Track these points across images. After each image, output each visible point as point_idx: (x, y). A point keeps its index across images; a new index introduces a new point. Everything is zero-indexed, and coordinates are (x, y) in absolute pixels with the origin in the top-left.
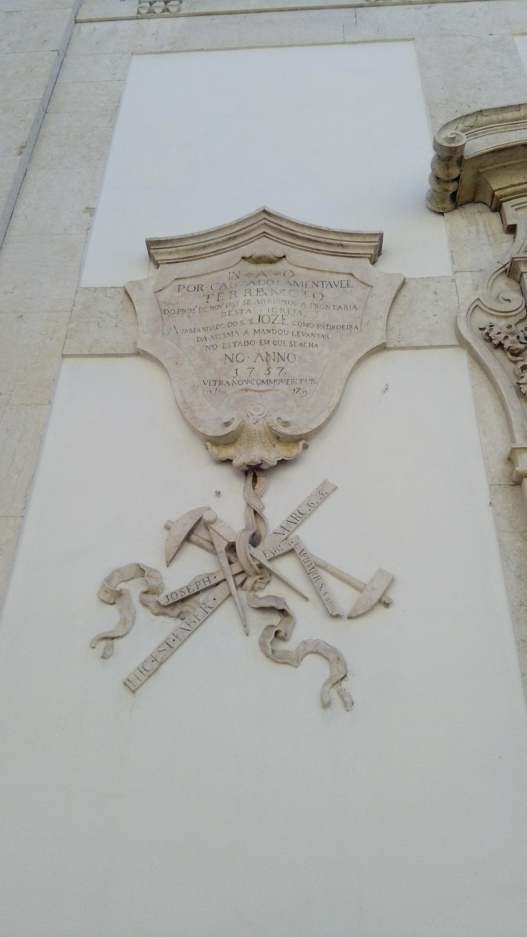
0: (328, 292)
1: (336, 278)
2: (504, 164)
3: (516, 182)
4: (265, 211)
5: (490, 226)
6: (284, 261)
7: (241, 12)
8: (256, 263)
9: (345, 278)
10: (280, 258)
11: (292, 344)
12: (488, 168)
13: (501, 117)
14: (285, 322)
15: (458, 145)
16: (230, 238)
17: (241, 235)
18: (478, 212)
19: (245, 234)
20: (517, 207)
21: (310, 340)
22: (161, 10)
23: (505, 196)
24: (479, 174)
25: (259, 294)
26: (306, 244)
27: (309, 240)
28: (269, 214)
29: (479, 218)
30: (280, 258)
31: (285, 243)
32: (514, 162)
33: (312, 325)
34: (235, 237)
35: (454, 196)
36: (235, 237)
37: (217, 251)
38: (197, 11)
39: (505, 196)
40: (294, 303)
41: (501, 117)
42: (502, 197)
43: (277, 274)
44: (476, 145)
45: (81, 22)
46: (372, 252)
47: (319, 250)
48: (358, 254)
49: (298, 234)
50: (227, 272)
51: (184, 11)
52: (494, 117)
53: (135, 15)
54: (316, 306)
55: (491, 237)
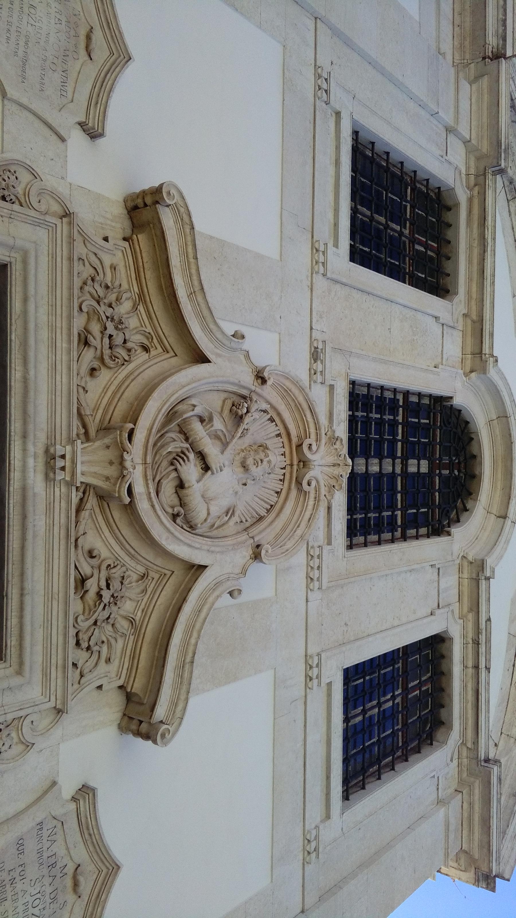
0: (57, 77)
1: (70, 89)
2: (156, 245)
3: (144, 255)
4: (130, 59)
5: (110, 230)
6: (87, 58)
7: (314, 145)
8: (87, 36)
9: (70, 95)
10: (90, 56)
11: (9, 23)
12: (153, 231)
13: (189, 243)
14: (29, 25)
15: (166, 199)
16: (108, 23)
17: (111, 33)
18: (124, 228)
19: (112, 36)
20: (124, 252)
21: (13, 39)
22: (320, 84)
23: (133, 244)
24: (149, 223)
25: (57, 20)
26: (100, 80)
27: (103, 82)
28: (127, 61)
29: (119, 225)
30: (90, 56)
31: (103, 65)
32: (158, 253)
33: (26, 47)
34: (110, 29)
35: (136, 208)
36: (110, 29)
37: (99, 11)
38: (317, 112)
39: (133, 244)
40: (47, 42)
41: (189, 243)
42: (132, 240)
43: (76, 46)
44: (168, 219)
45: (316, 23)
46: (90, 125)
47: (95, 88)
48: (89, 114)
49: (109, 75)
50: (80, 9)
51: (318, 102)
52: (189, 238)
53: (318, 64)
54: (45, 61)
55: (100, 225)
